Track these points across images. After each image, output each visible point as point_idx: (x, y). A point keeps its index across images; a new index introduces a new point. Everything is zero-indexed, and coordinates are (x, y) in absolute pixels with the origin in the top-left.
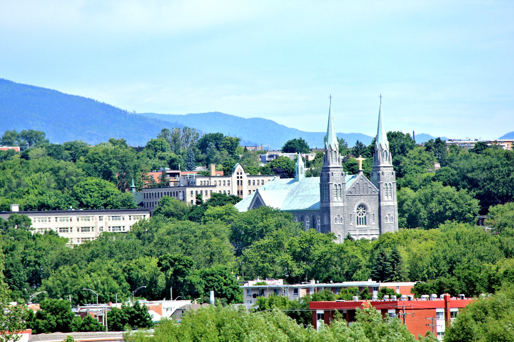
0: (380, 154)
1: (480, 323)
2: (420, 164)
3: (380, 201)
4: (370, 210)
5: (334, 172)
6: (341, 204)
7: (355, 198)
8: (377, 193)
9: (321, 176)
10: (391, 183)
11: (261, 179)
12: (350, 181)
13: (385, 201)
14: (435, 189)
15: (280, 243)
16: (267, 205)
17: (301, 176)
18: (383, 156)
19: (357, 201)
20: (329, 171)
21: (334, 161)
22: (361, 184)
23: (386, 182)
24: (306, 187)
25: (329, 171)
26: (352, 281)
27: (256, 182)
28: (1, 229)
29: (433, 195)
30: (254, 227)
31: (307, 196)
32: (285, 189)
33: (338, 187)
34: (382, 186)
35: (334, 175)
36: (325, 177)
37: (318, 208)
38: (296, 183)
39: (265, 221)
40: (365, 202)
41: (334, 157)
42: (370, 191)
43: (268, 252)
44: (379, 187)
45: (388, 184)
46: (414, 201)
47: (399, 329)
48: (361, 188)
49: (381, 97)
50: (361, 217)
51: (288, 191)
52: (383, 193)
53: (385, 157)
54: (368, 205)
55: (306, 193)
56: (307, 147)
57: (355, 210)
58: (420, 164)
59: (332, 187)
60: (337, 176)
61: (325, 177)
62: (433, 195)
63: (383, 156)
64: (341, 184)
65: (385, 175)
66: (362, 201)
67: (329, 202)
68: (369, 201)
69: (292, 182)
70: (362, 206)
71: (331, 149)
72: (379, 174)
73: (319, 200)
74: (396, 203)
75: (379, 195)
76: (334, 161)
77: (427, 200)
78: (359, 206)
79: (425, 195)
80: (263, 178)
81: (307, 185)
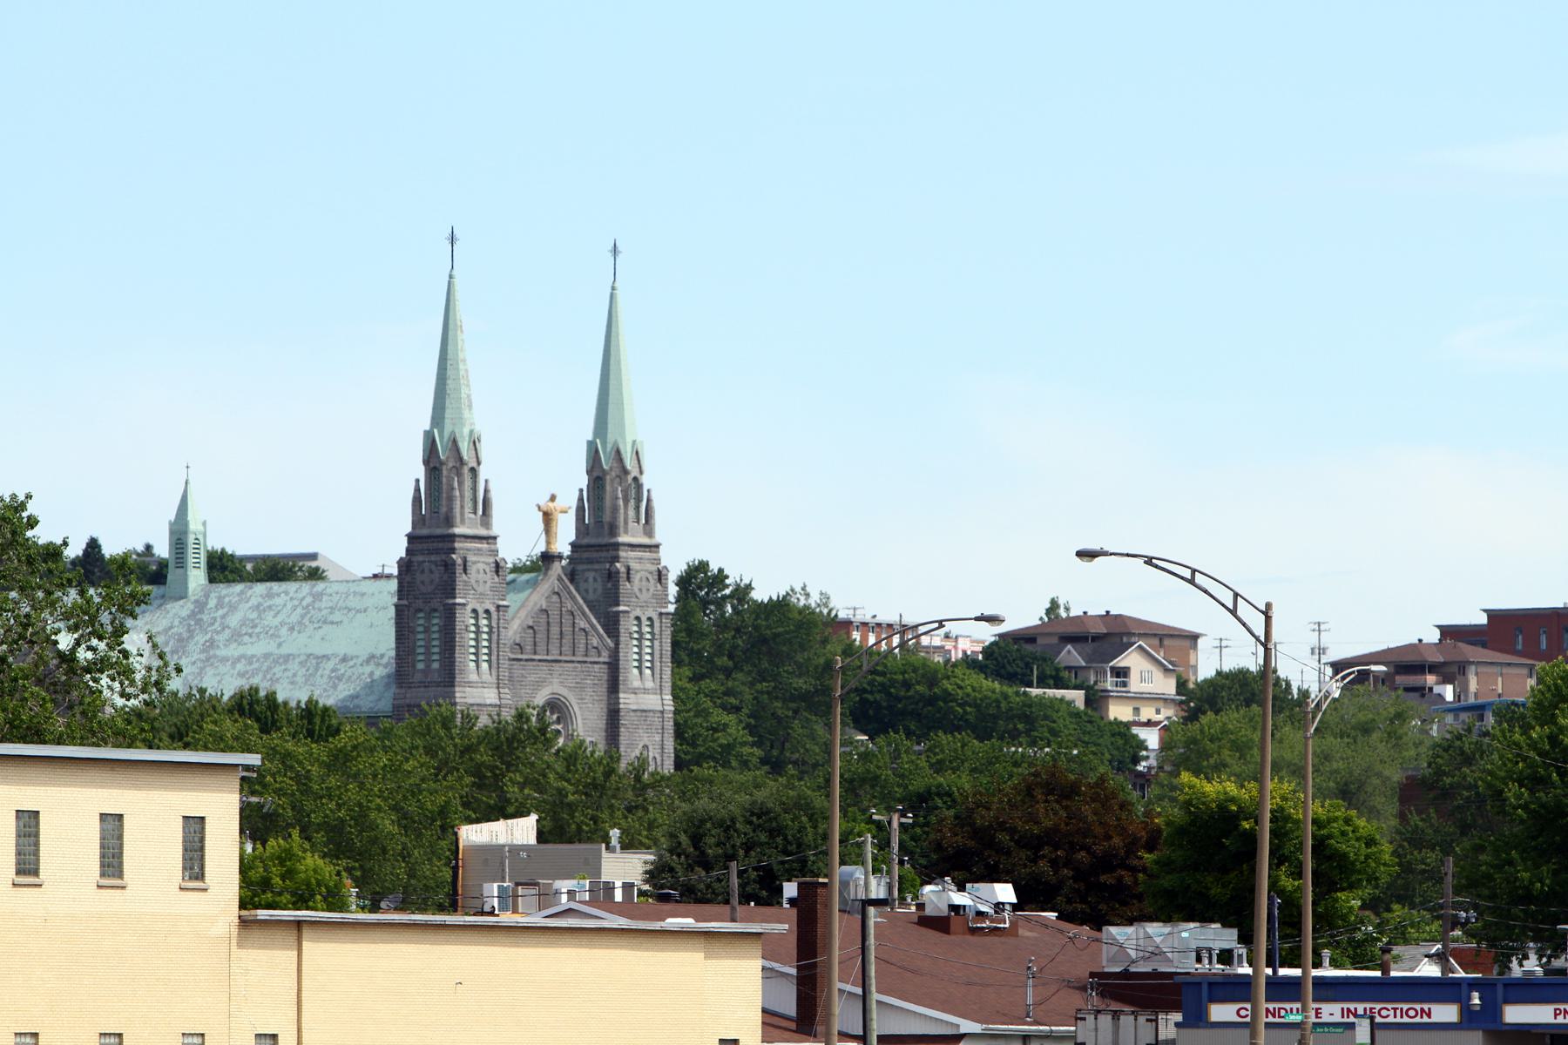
1: (303, 658)
5: (471, 558)
8: (605, 658)
10: (655, 617)
13: (635, 692)
20: (453, 550)
23: (638, 612)
25: (453, 550)
26: (44, 742)
34: (628, 626)
35: (472, 569)
40: (564, 692)
42: (581, 647)
45: (644, 619)
47: (1113, 909)
49: (615, 250)
52: (629, 653)
53: (632, 503)
54: (573, 700)
60: (481, 576)
64: (492, 609)
65: (636, 578)
71: (461, 459)
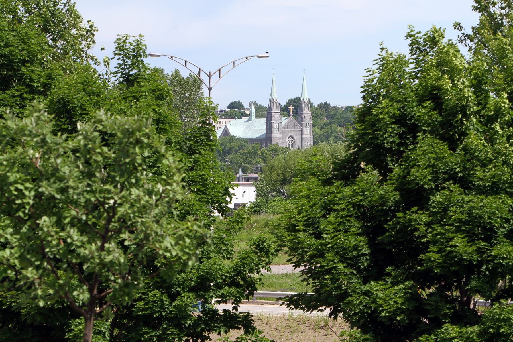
0: (303, 105)
2: (316, 117)
3: (302, 134)
4: (296, 140)
6: (279, 135)
7: (287, 132)
9: (267, 117)
11: (224, 120)
12: (284, 121)
14: (333, 129)
15: (255, 152)
16: (232, 135)
17: (253, 117)
18: (305, 106)
19: (288, 134)
21: (275, 109)
22: (291, 124)
24: (257, 124)
27: (221, 122)
28: (2, 266)
29: (331, 132)
30: (225, 147)
31: (257, 130)
32: (243, 125)
33: (277, 125)
34: (304, 125)
36: (269, 118)
37: (264, 137)
38: (250, 122)
39: (231, 144)
41: (275, 106)
43: (247, 157)
44: (302, 126)
46: (320, 136)
48: (291, 126)
50: (290, 143)
51: (245, 127)
52: (305, 129)
55: (256, 128)
56: (243, 106)
57: (287, 139)
58: (316, 117)
59: (274, 125)
61: (269, 118)
62: (331, 132)
63: (305, 106)
66: (291, 134)
67: (271, 133)
68: (296, 134)
69: (247, 121)
70: (291, 137)
72: (302, 118)
73: (265, 132)
74: (312, 136)
75: (302, 131)
76: (275, 109)
77: (328, 135)
78: (289, 137)
79: (327, 132)
80: (225, 120)
81: (257, 123)
